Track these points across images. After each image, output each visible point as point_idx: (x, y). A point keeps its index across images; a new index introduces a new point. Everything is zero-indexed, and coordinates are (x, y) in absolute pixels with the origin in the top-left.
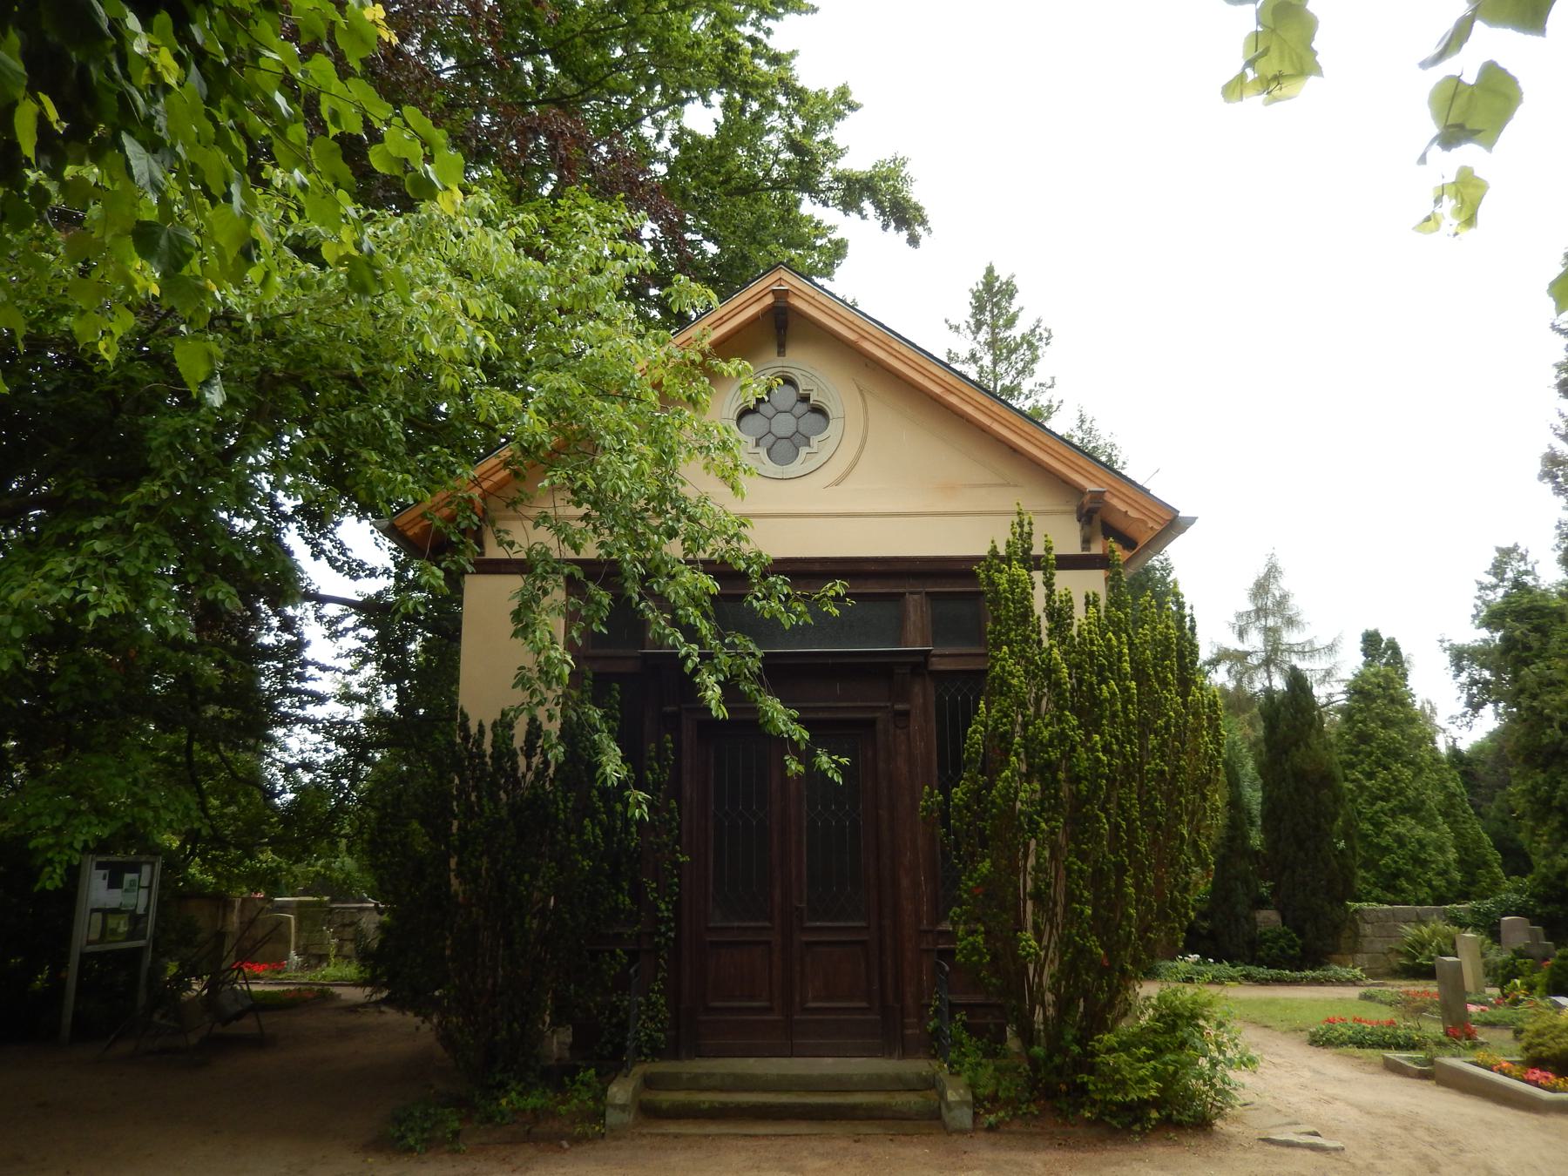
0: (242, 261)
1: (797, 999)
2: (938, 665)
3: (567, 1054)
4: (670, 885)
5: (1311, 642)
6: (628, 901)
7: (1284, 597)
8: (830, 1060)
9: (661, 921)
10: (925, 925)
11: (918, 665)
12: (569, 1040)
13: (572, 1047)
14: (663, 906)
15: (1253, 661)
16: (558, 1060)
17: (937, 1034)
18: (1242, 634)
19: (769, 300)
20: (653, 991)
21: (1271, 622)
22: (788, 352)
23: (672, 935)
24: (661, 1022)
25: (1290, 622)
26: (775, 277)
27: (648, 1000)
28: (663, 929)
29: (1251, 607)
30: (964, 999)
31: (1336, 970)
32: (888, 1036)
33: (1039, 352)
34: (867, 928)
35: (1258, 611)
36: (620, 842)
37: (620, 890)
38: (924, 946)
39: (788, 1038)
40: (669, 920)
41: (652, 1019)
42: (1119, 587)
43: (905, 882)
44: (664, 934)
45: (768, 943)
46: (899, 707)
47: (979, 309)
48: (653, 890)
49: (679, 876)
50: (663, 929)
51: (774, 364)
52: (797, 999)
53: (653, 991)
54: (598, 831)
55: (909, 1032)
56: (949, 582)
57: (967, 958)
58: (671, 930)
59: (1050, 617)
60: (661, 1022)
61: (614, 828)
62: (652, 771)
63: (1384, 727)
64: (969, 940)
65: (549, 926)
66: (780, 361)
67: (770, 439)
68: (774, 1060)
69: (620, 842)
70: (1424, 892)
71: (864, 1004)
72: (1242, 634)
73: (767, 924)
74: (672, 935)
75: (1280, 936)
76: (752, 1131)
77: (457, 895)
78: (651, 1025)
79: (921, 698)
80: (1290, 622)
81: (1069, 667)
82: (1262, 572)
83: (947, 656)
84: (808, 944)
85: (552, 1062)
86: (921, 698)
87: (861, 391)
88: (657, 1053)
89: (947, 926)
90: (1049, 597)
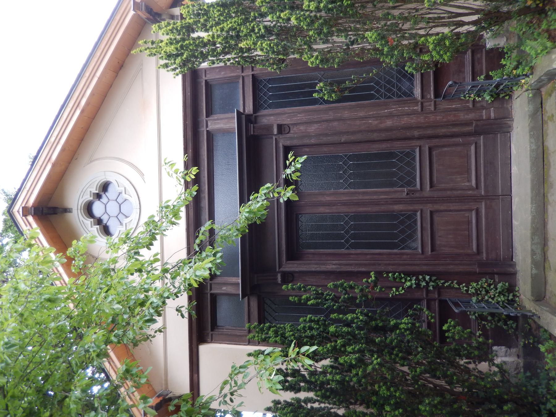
2: (249, 109)
3: (514, 350)
4: (395, 279)
6: (405, 320)
8: (514, 169)
9: (418, 285)
10: (419, 108)
12: (503, 348)
13: (509, 347)
14: (408, 284)
16: (518, 356)
17: (496, 96)
19: (30, 218)
22: (70, 207)
23: (427, 278)
24: (489, 285)
26: (16, 214)
27: (473, 294)
28: (424, 284)
30: (469, 78)
34: (420, 147)
36: (360, 328)
37: (396, 326)
38: (432, 108)
39: (498, 197)
40: (417, 279)
41: (487, 292)
43: (389, 123)
44: (427, 283)
45: (431, 212)
46: (275, 131)
49: (388, 273)
50: (424, 284)
51: (77, 218)
53: (467, 291)
54: (349, 349)
55: (492, 115)
57: (447, 49)
58: (424, 279)
60: (489, 285)
61: (348, 333)
62: (308, 299)
66: (75, 211)
67: (120, 216)
68: (514, 208)
69: (360, 328)
71: (473, 148)
73: (419, 214)
74: (427, 278)
77: (405, 57)
78: (492, 293)
79: (271, 117)
81: (506, 356)
84: (431, 186)
85: (521, 362)
86: (271, 117)
87: (91, 162)
88: (511, 289)
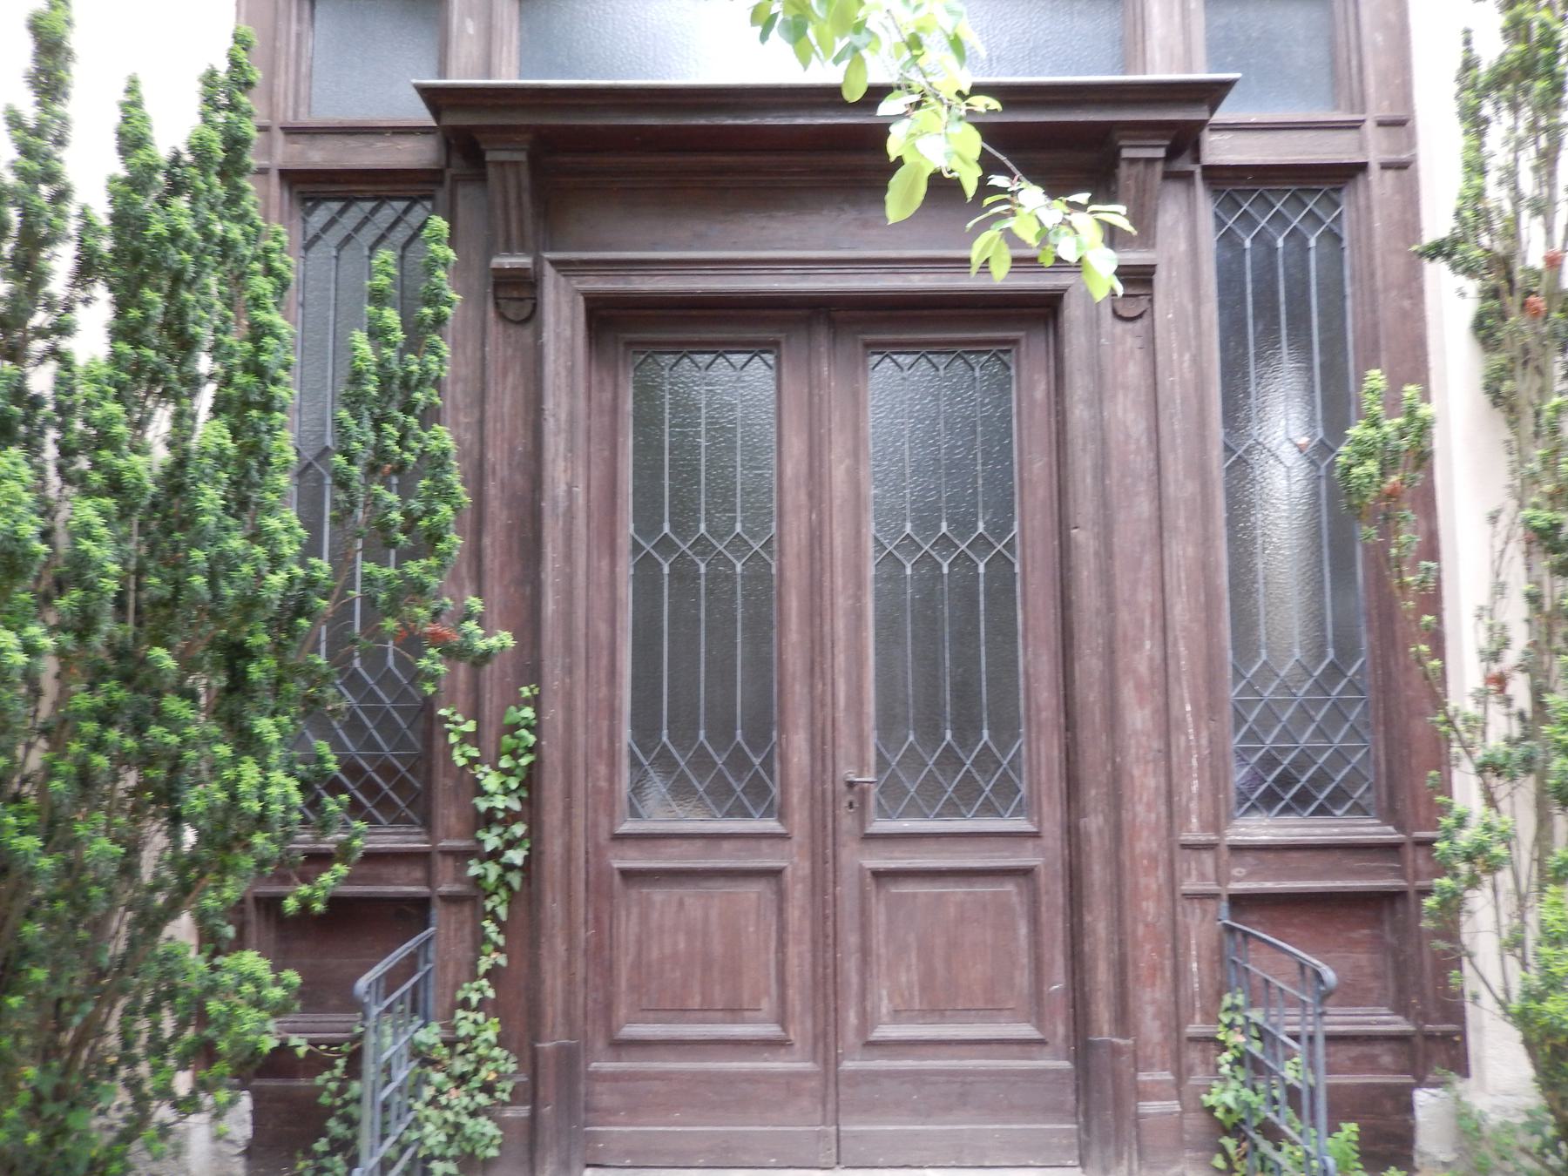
0: (55, 21)
1: (852, 1018)
9: (488, 819)
10: (1194, 832)
14: (491, 782)
20: (465, 1004)
24: (488, 1088)
38: (1190, 885)
40: (511, 817)
42: (1483, 172)
43: (1138, 717)
45: (776, 874)
48: (465, 738)
49: (536, 702)
52: (852, 1018)
53: (465, 1004)
55: (1150, 1107)
60: (488, 1088)
63: (216, 1105)
65: (189, 836)
71: (1026, 1031)
73: (772, 825)
76: (696, 337)
78: (458, 1098)
84: (878, 875)
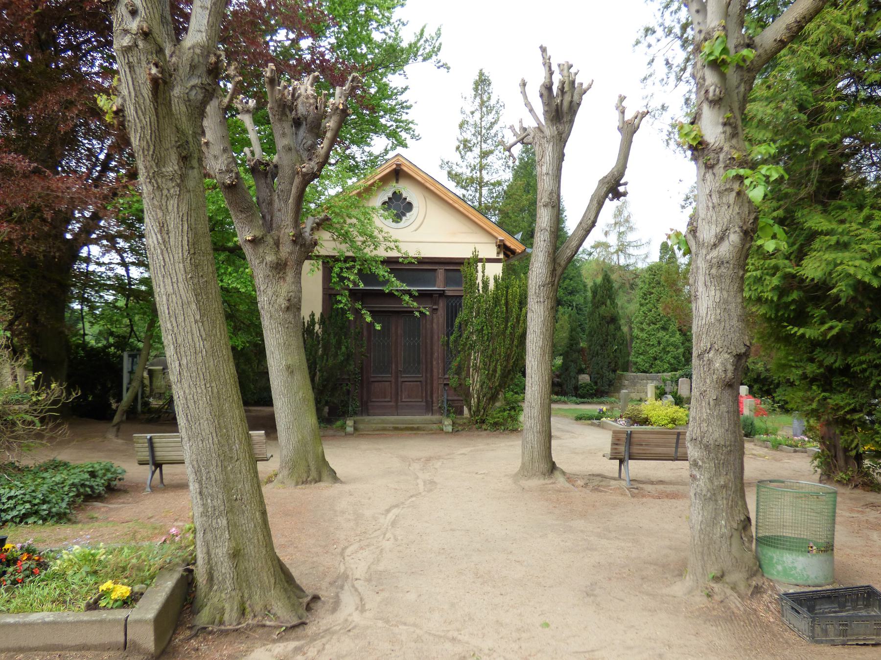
5: (640, 240)
7: (629, 216)
11: (441, 294)
15: (612, 250)
18: (606, 234)
19: (394, 166)
21: (622, 229)
25: (631, 229)
29: (613, 222)
31: (603, 399)
32: (429, 408)
33: (501, 113)
35: (616, 224)
43: (434, 363)
47: (476, 89)
56: (455, 267)
59: (483, 283)
64: (454, 381)
70: (666, 366)
72: (606, 234)
75: (587, 385)
80: (631, 229)
82: (339, 474)
83: (451, 290)
89: (447, 376)
90: (483, 276)
